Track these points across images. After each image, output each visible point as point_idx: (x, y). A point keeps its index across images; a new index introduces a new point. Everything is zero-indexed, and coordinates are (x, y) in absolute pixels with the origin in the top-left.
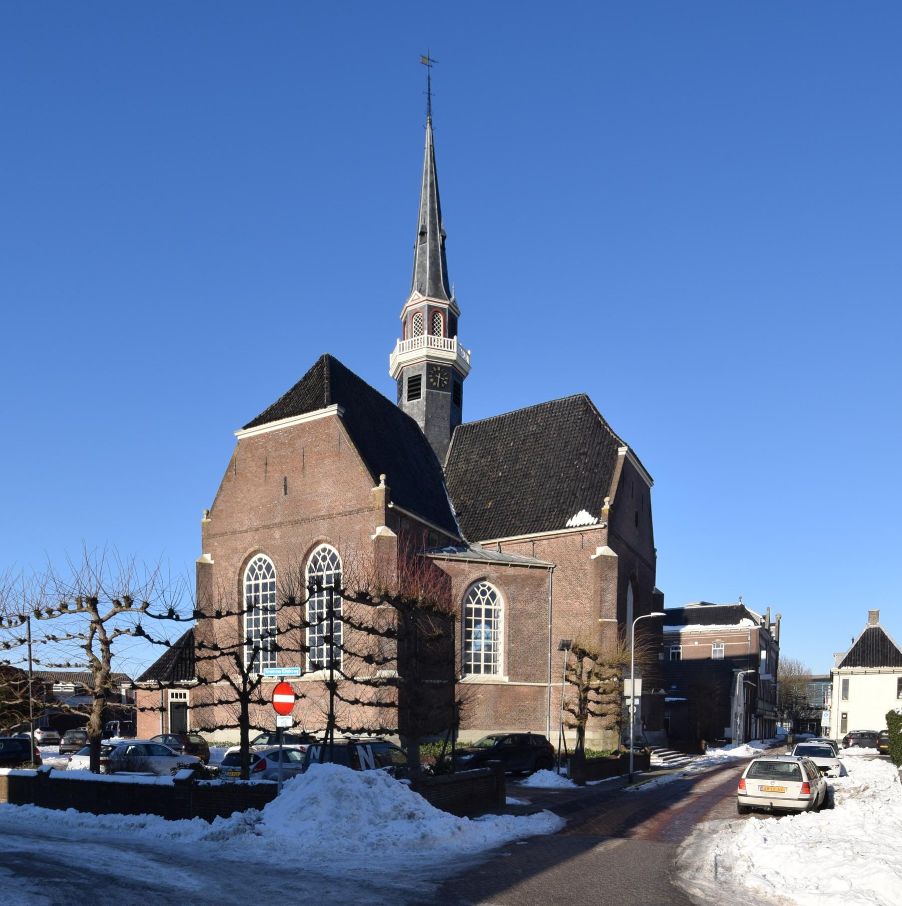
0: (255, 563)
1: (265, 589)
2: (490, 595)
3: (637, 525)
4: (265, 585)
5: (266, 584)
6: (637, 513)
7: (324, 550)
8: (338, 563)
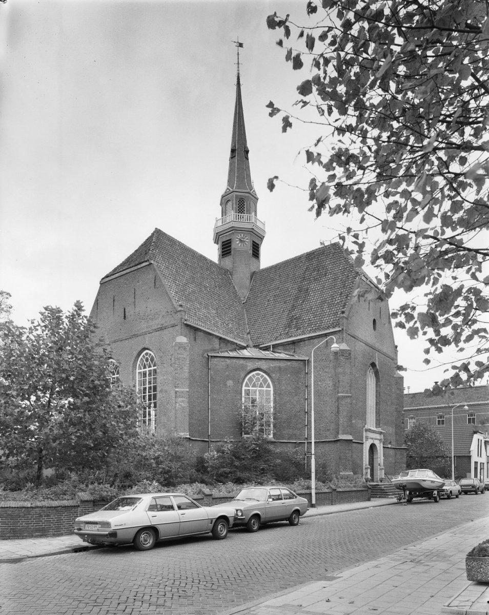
0: (144, 356)
1: (150, 375)
2: (262, 381)
3: (375, 328)
4: (150, 371)
5: (150, 371)
6: (374, 321)
7: (147, 354)
8: (269, 383)
